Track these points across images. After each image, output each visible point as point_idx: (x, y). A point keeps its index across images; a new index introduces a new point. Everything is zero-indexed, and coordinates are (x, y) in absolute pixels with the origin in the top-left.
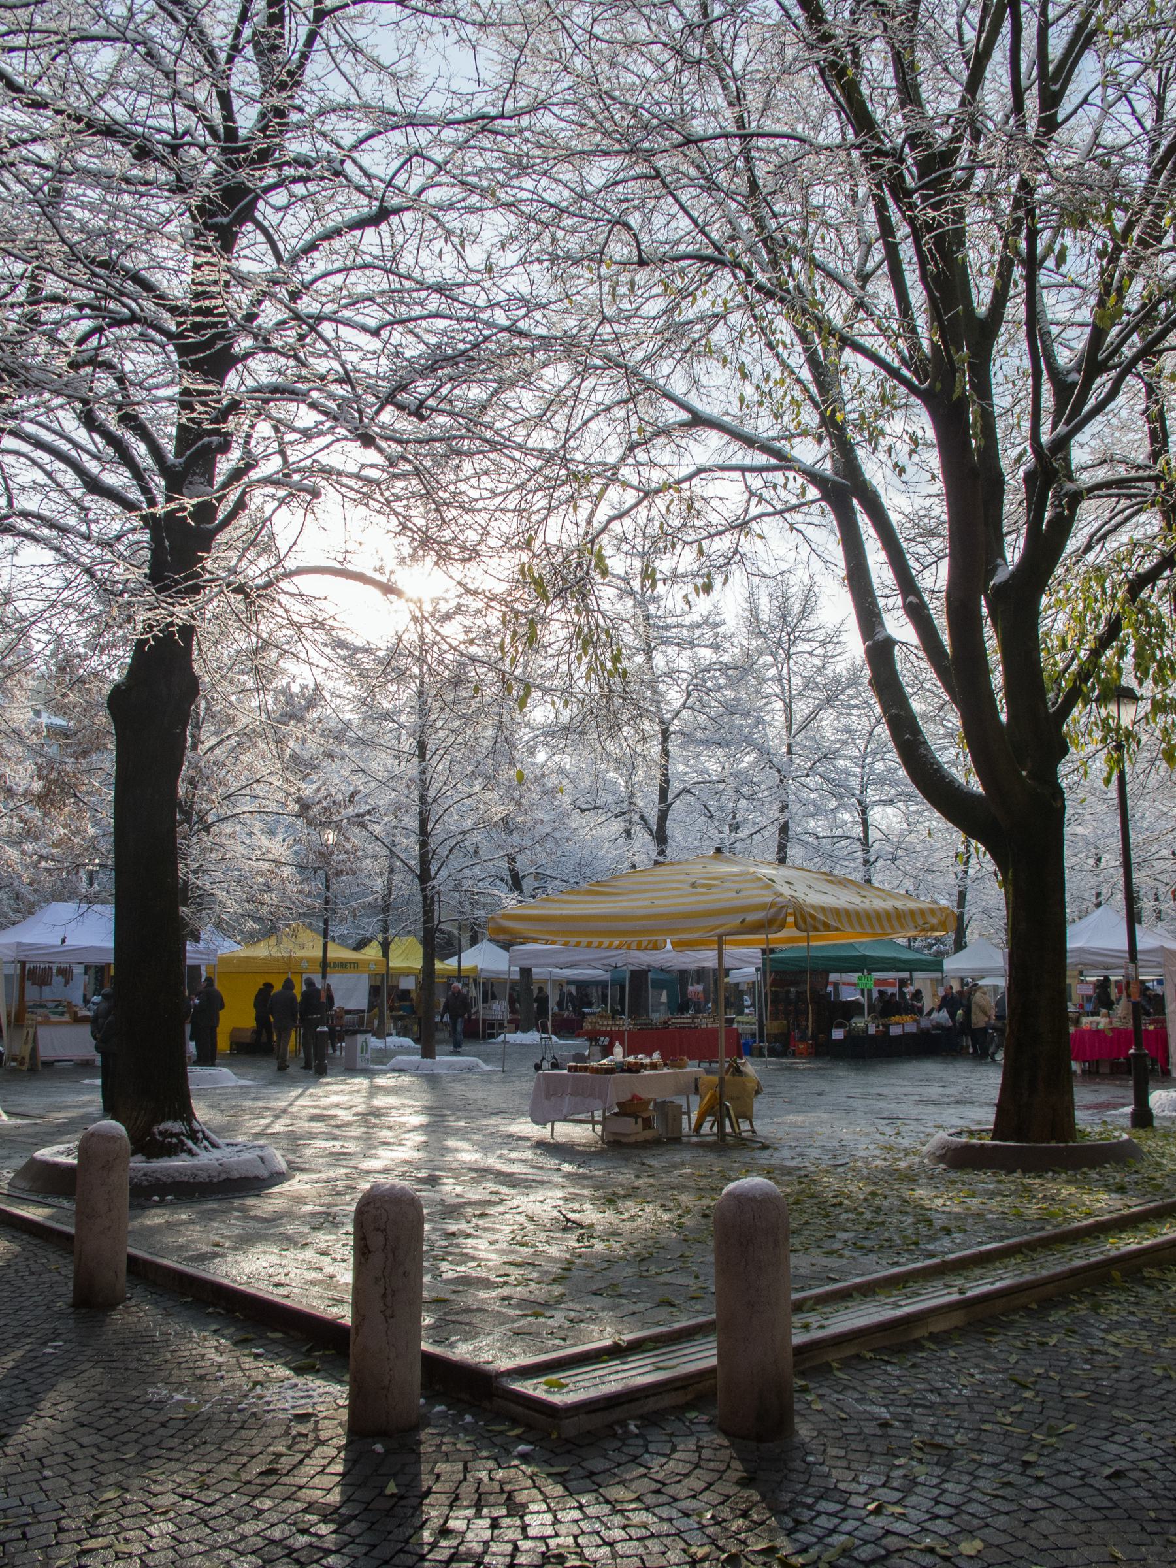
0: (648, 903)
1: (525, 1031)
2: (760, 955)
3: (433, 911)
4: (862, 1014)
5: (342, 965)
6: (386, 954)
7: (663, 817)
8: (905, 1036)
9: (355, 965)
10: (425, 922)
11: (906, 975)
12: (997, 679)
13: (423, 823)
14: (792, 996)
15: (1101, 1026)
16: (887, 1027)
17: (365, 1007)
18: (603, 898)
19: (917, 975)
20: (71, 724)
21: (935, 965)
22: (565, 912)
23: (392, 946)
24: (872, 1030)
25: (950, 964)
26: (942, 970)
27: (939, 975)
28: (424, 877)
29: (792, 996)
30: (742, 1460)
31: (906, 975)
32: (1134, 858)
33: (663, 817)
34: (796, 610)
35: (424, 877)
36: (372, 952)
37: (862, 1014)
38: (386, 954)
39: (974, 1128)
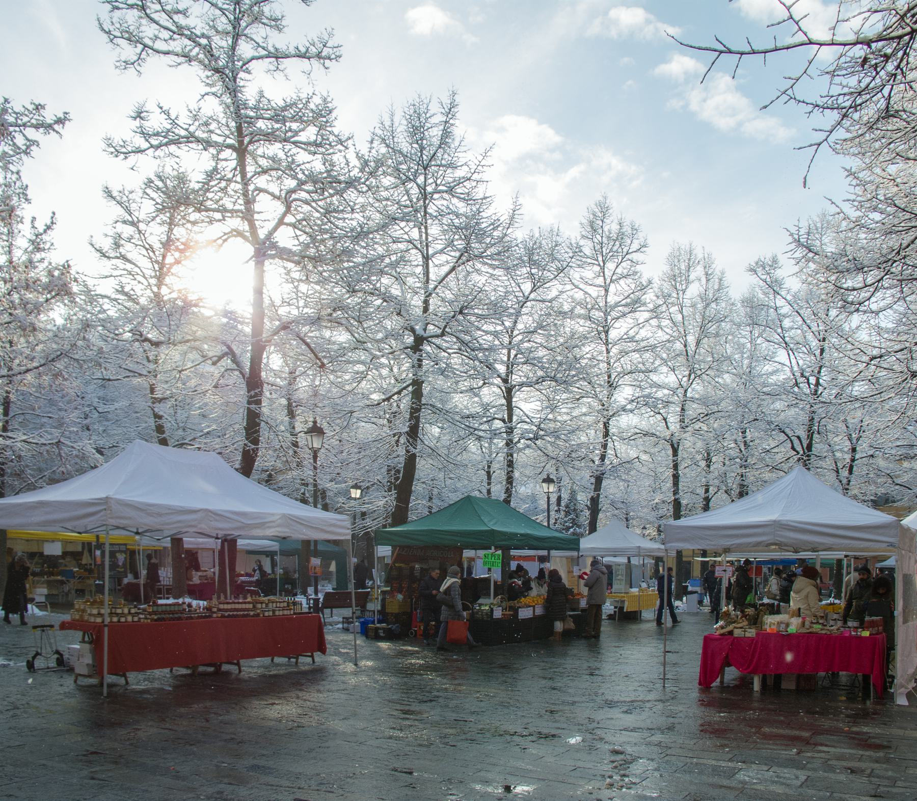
2: (348, 524)
4: (488, 595)
11: (544, 553)
12: (410, 648)
14: (417, 574)
15: (792, 629)
16: (516, 611)
19: (554, 553)
20: (902, 701)
21: (573, 544)
24: (498, 614)
25: (587, 543)
26: (578, 549)
27: (575, 554)
29: (417, 574)
31: (544, 553)
32: (546, 514)
34: (435, 133)
37: (488, 595)
39: (173, 148)
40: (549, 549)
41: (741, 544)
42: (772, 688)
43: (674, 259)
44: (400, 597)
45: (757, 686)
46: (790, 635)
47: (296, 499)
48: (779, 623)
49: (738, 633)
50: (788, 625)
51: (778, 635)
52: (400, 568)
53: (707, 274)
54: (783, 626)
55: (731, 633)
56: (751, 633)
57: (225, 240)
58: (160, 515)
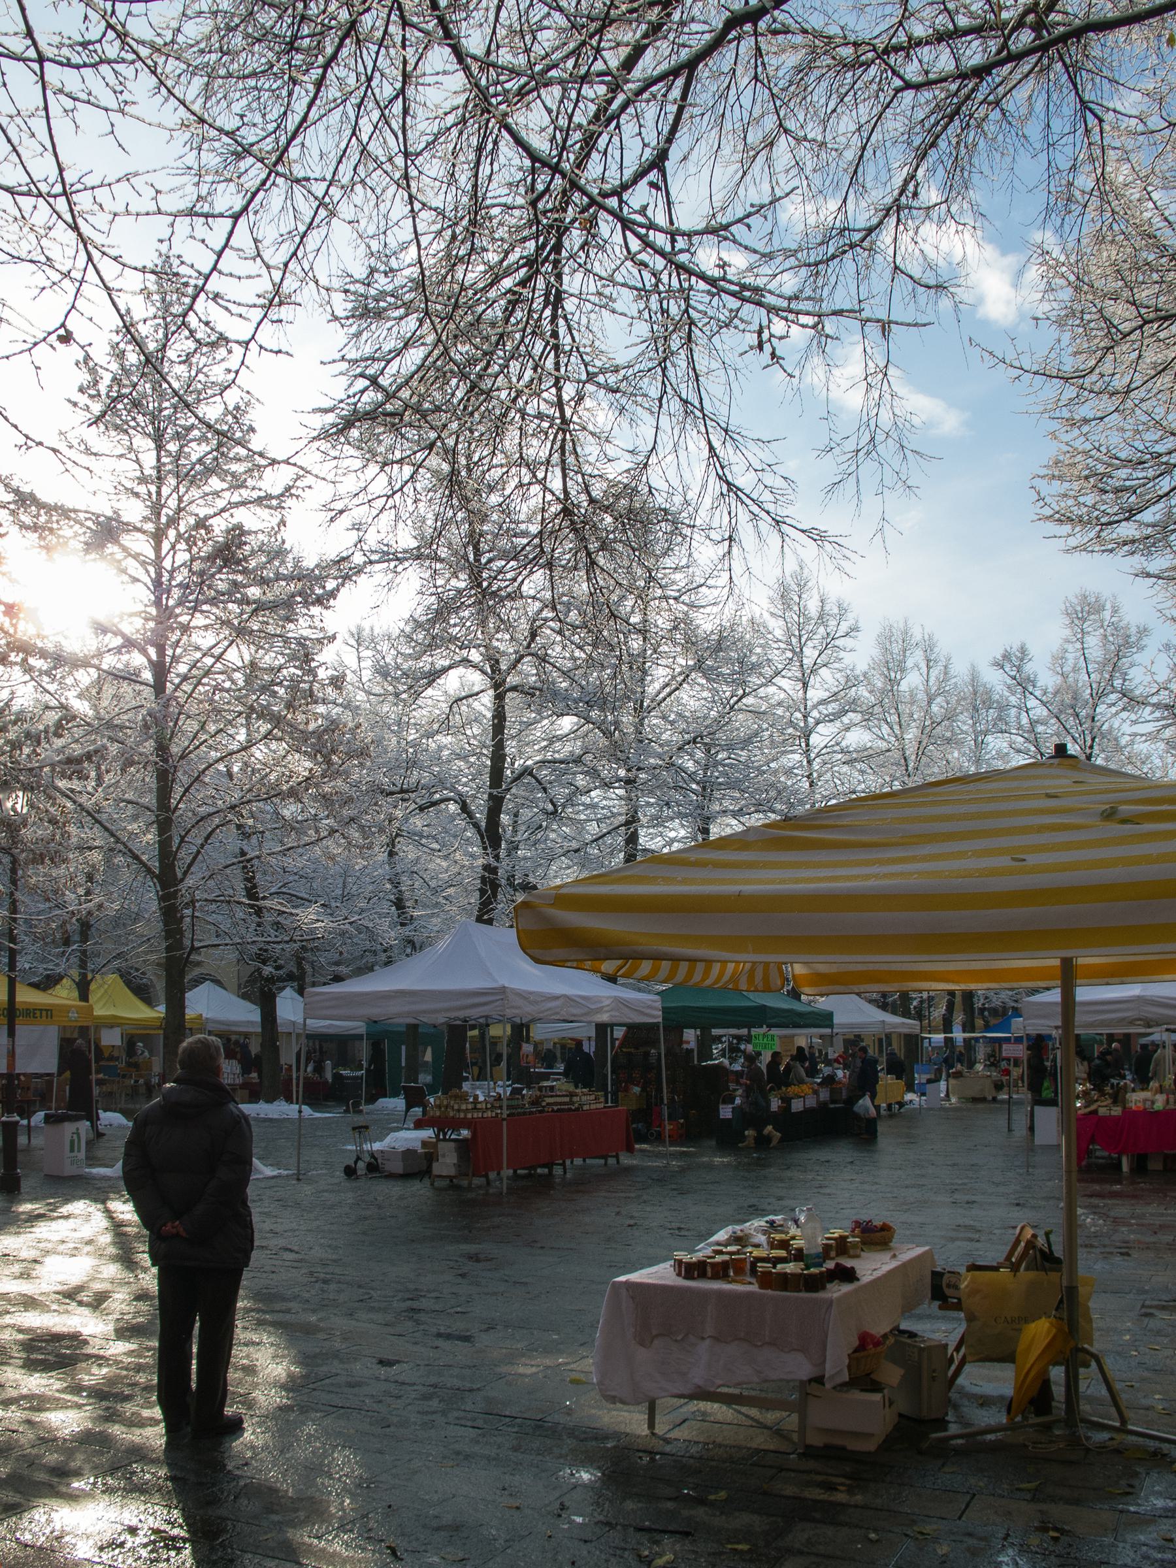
0: (1005, 861)
1: (270, 1100)
3: (181, 932)
5: (33, 1013)
6: (84, 996)
7: (495, 806)
8: (807, 1111)
9: (47, 1012)
10: (168, 949)
13: (164, 792)
17: (54, 1069)
18: (863, 855)
22: (748, 889)
23: (93, 986)
26: (831, 1026)
28: (167, 877)
30: (348, 1443)
31: (744, 1031)
33: (495, 806)
35: (167, 877)
36: (64, 995)
38: (84, 996)
40: (749, 1026)
41: (1103, 1021)
42: (1140, 1168)
43: (886, 639)
44: (637, 1090)
45: (1125, 1167)
46: (1158, 1113)
47: (870, 1001)
48: (1145, 1100)
49: (1102, 1112)
50: (1153, 1103)
51: (1145, 1113)
52: (629, 1054)
53: (928, 661)
54: (1148, 1104)
55: (1095, 1112)
56: (1117, 1111)
57: (75, 511)
58: (536, 1002)
